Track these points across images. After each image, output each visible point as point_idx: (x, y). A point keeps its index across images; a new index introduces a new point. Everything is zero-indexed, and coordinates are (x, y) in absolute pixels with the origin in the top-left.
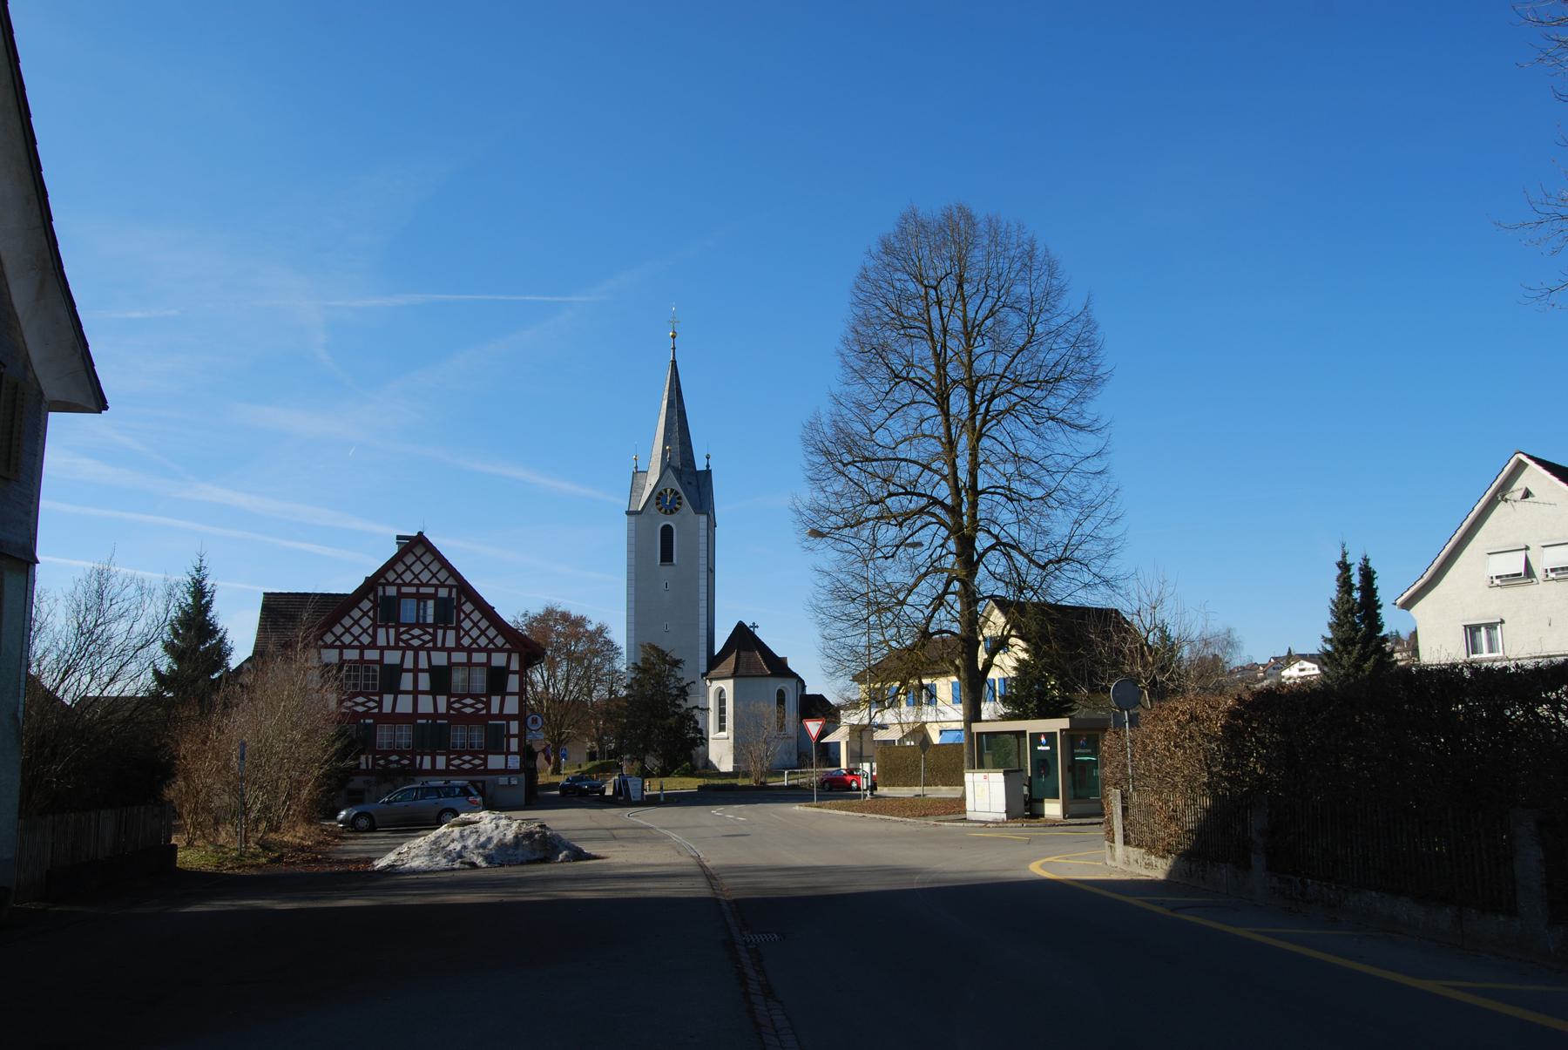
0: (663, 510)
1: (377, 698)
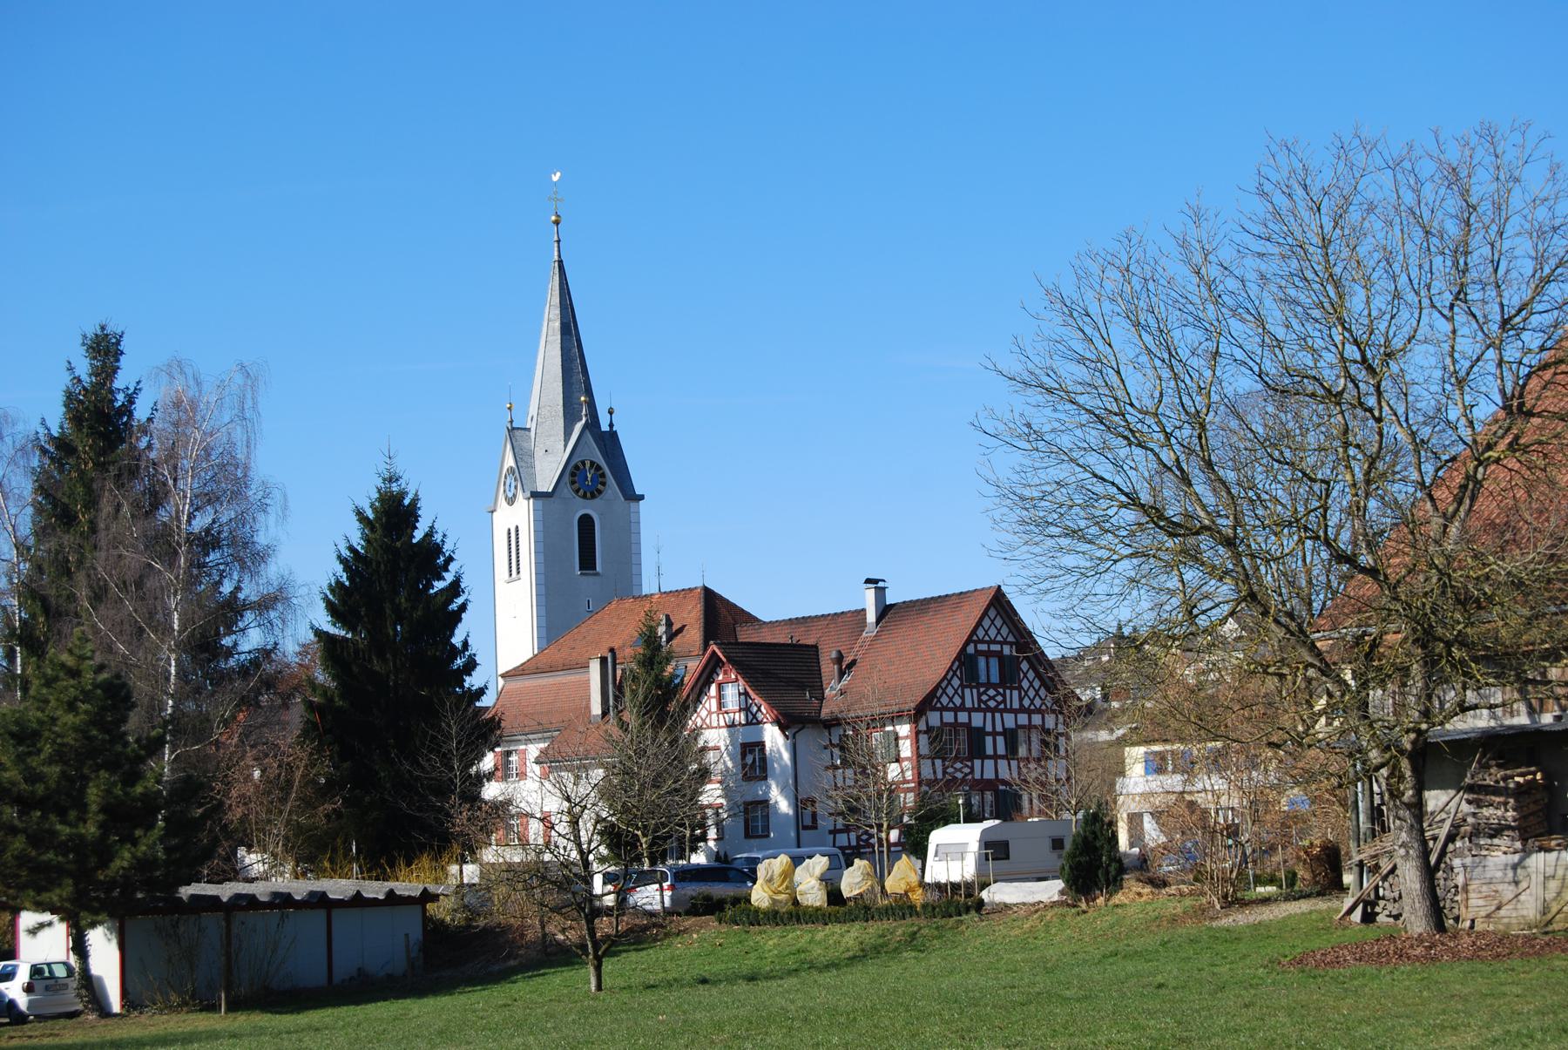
0: (581, 492)
1: (969, 764)
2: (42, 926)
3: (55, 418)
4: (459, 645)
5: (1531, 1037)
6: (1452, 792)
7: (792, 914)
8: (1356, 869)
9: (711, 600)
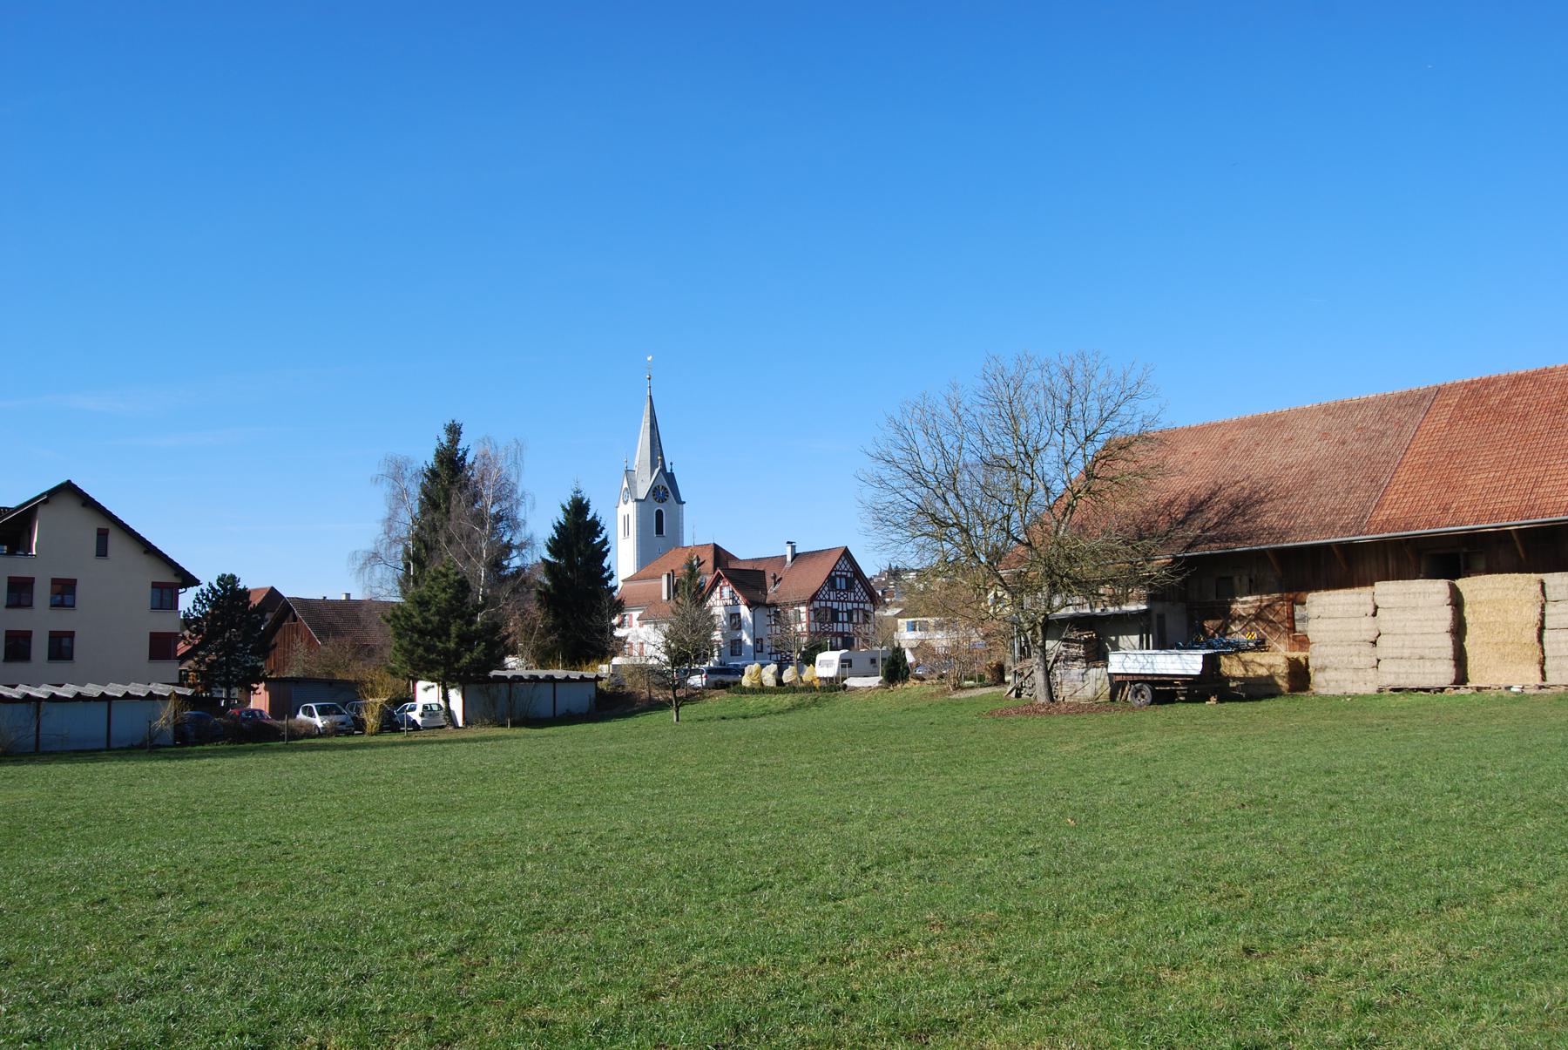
2: (429, 687)
3: (431, 460)
4: (606, 567)
5: (1101, 746)
6: (1056, 642)
7: (761, 689)
8: (1013, 674)
9: (716, 548)
